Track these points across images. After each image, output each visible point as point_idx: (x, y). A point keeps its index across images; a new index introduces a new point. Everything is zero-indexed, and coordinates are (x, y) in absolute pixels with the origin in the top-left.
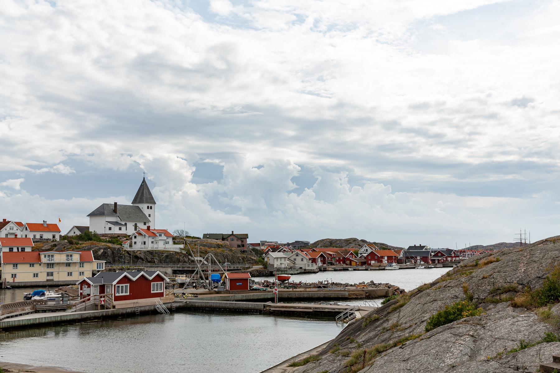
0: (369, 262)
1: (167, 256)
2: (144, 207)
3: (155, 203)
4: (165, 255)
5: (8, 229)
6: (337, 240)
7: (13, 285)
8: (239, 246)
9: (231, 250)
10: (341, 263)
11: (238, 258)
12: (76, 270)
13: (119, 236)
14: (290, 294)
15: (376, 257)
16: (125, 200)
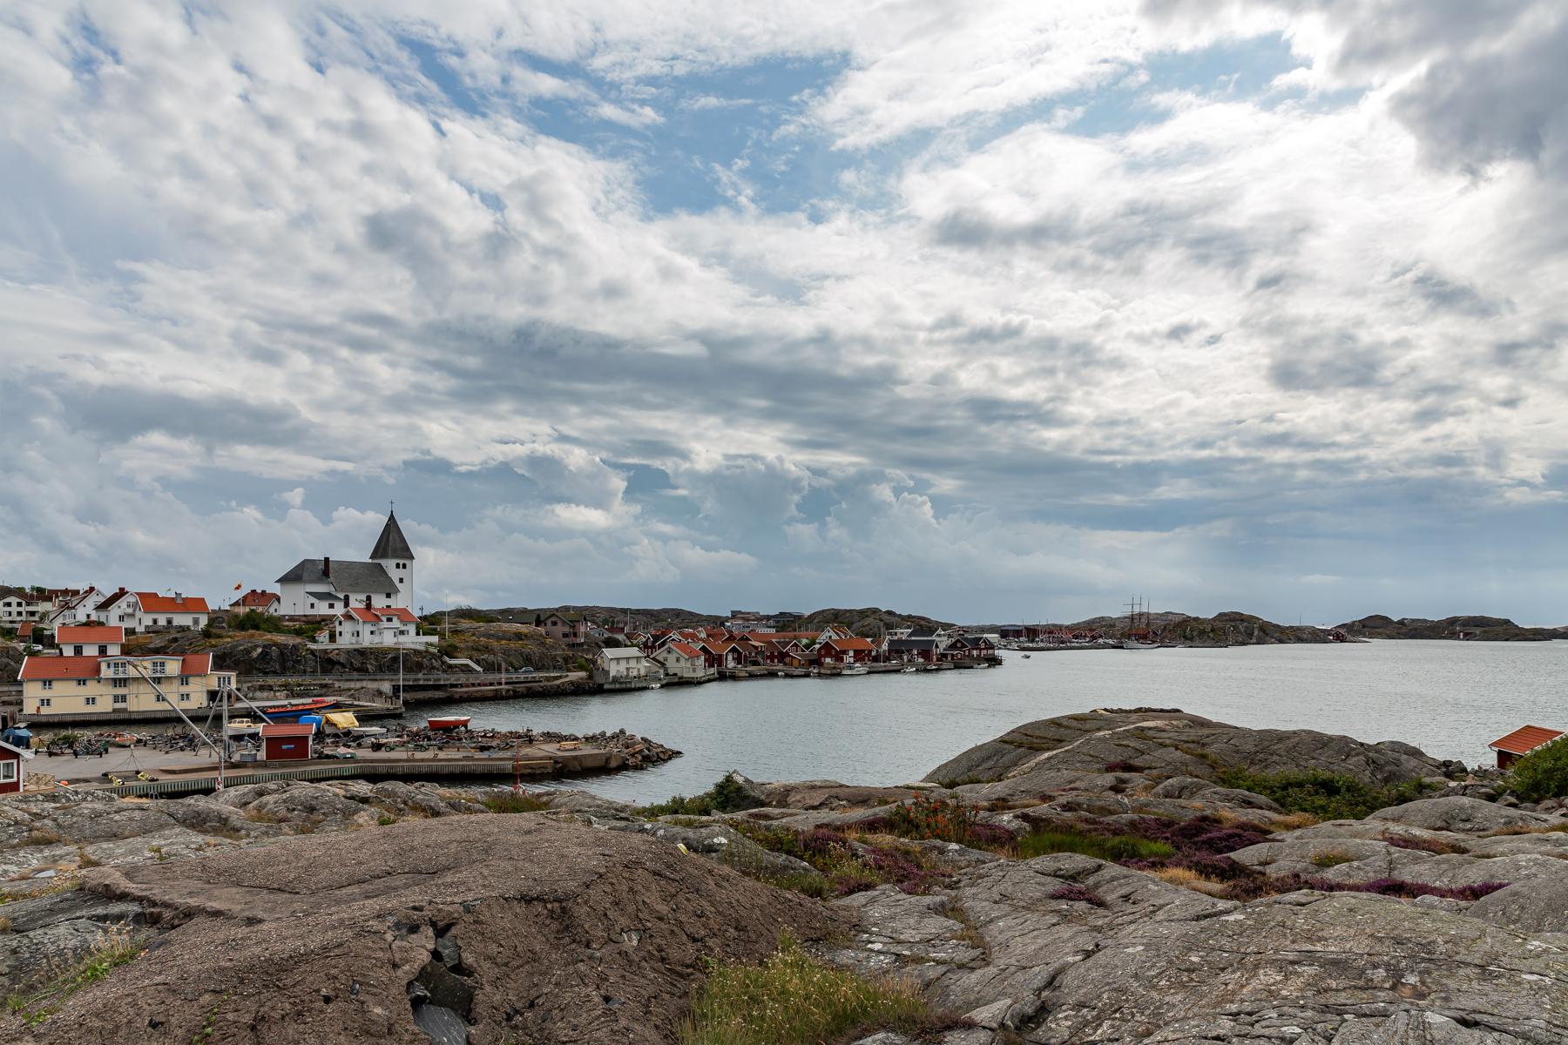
2: (389, 565)
5: (124, 605)
7: (36, 719)
8: (565, 635)
9: (543, 644)
12: (172, 692)
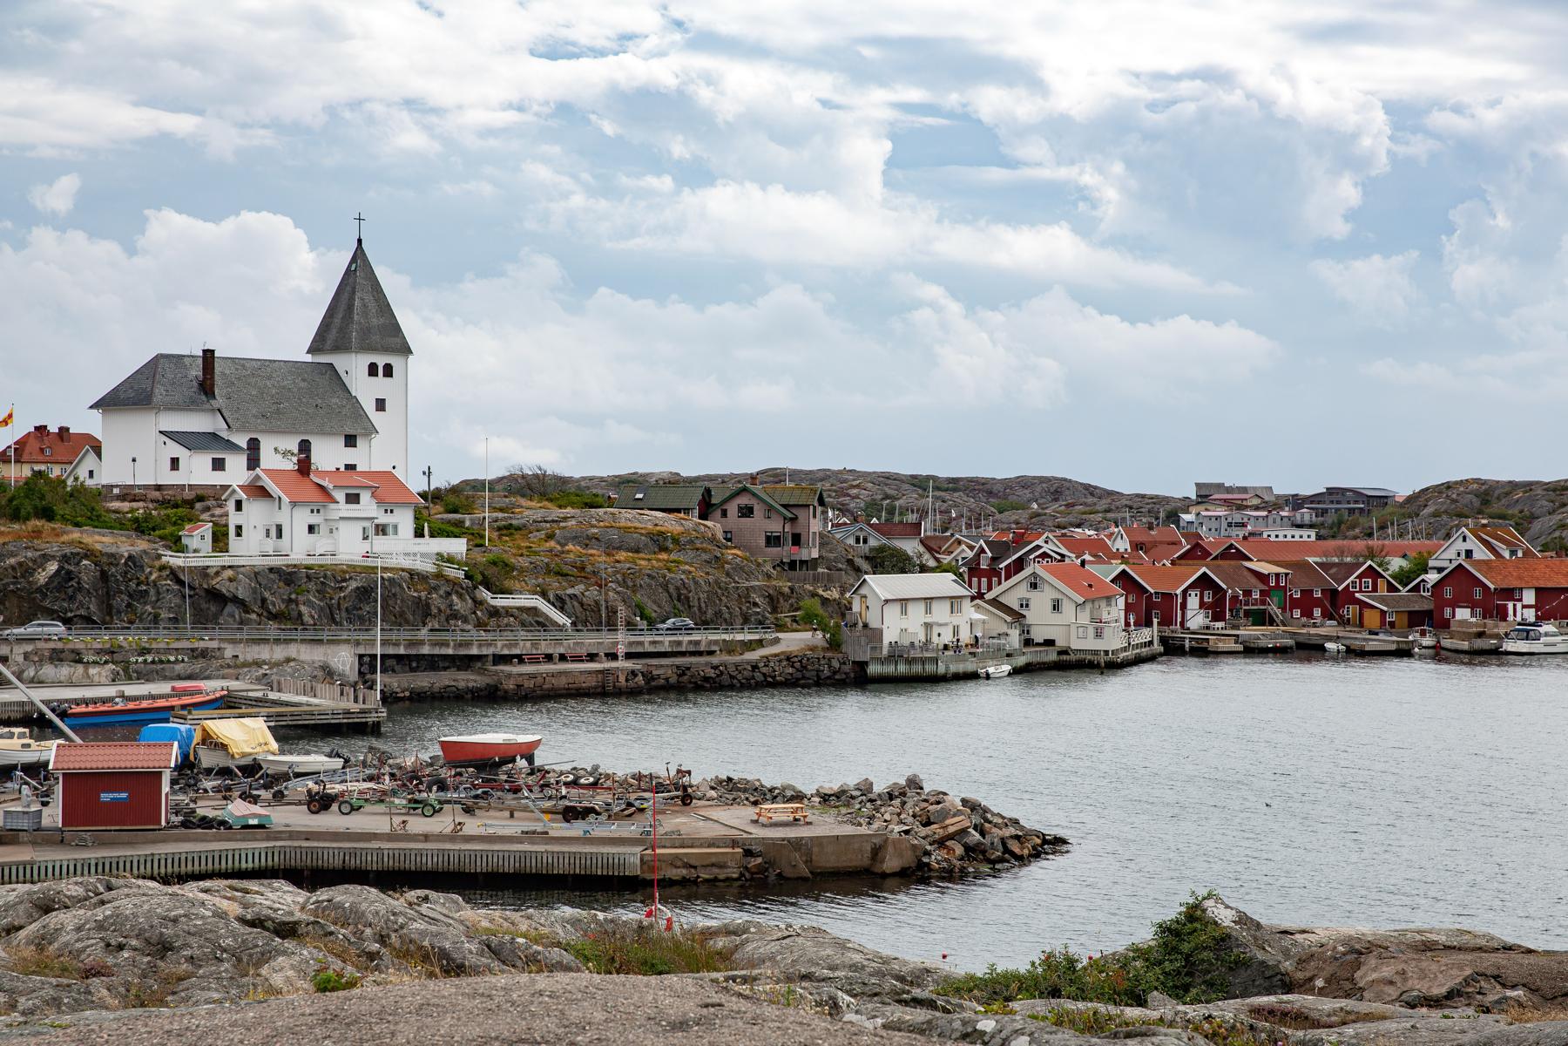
0: (1448, 611)
1: (365, 593)
2: (353, 367)
3: (406, 350)
4: (354, 585)
6: (1514, 485)
8: (773, 541)
10: (1317, 612)
11: (745, 596)
13: (200, 499)
14: (354, 853)
15: (1478, 594)
16: (283, 333)
